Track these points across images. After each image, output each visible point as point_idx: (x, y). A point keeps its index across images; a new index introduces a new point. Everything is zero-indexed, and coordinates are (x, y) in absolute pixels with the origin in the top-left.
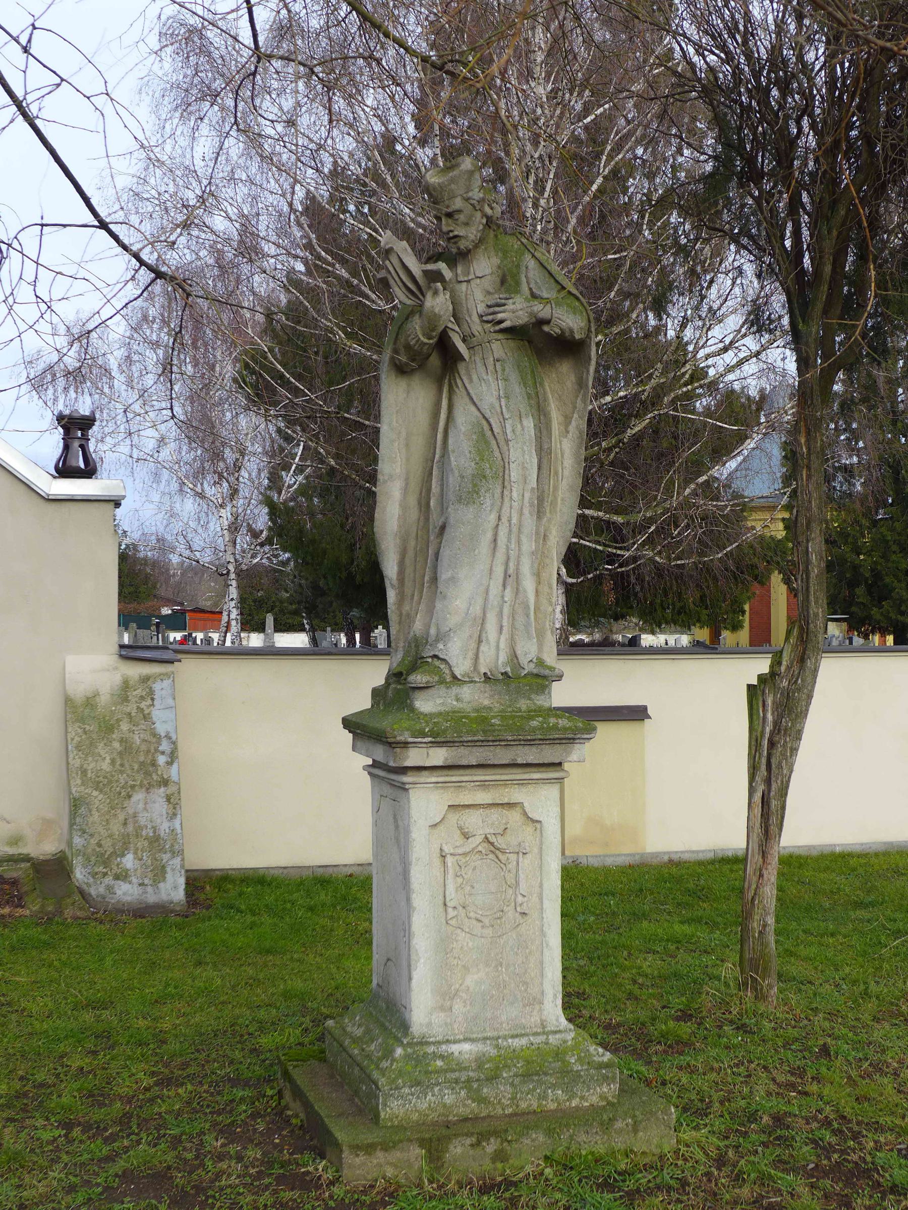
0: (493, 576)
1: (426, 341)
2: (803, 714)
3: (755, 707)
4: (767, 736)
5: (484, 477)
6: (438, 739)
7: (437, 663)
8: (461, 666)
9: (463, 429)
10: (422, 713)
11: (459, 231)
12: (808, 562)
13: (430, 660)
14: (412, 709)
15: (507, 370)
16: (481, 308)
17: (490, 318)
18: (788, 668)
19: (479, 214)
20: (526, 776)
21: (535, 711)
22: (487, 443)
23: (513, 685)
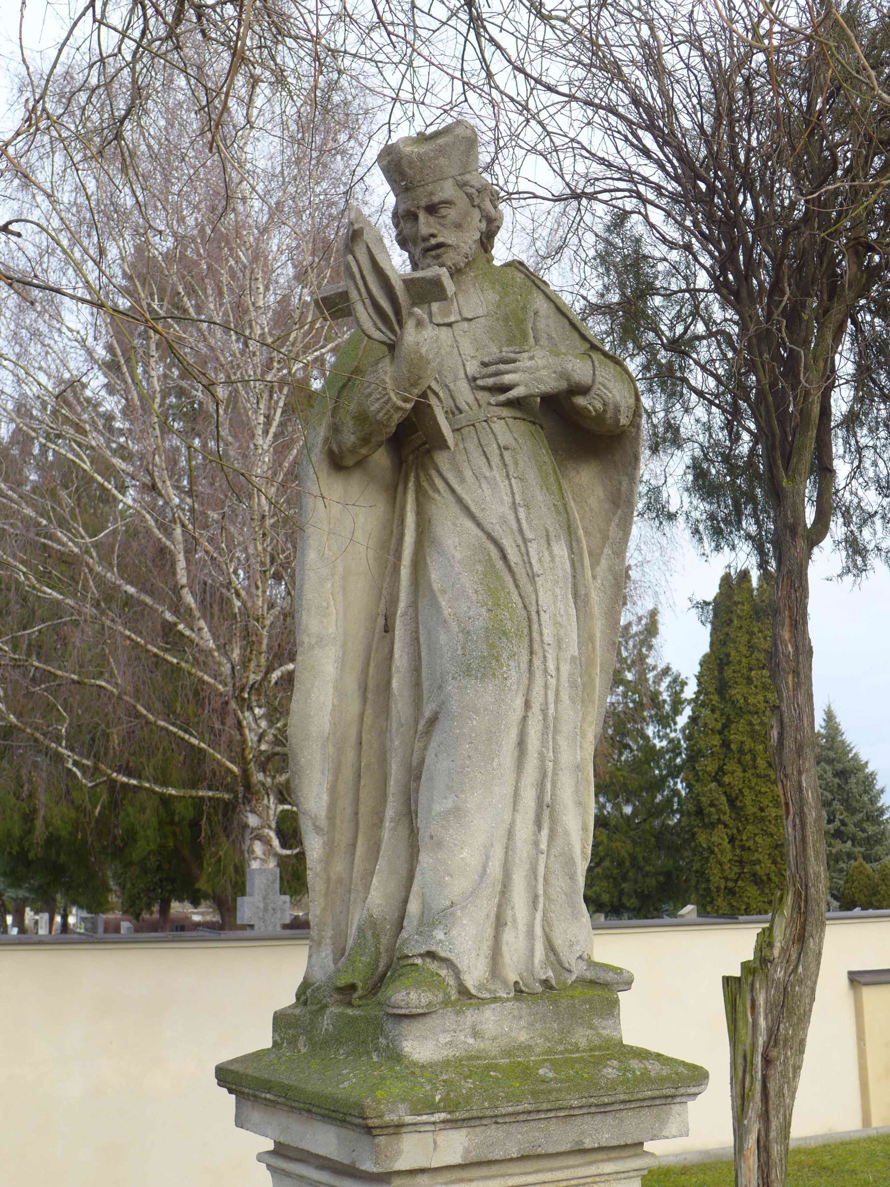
0: (520, 807)
1: (400, 403)
2: (805, 1018)
3: (740, 1008)
4: (760, 1050)
5: (504, 633)
6: (458, 1115)
7: (433, 966)
8: (474, 973)
9: (458, 556)
10: (415, 1064)
11: (447, 237)
12: (802, 801)
13: (419, 961)
14: (395, 1056)
15: (521, 464)
16: (472, 368)
17: (490, 381)
18: (783, 950)
19: (476, 214)
20: (592, 1170)
21: (600, 1048)
22: (499, 578)
23: (564, 1003)
